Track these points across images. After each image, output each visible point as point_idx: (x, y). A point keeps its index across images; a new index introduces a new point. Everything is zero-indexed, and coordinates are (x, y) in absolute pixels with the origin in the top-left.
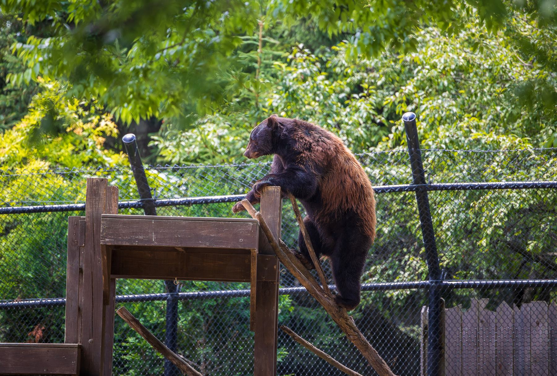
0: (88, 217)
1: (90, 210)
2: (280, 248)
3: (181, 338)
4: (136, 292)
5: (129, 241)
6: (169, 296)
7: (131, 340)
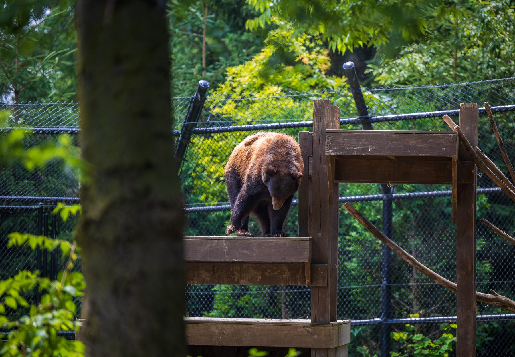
0: (315, 132)
1: (316, 127)
2: (477, 155)
3: (395, 232)
4: (356, 194)
5: (349, 151)
6: (385, 197)
7: (354, 234)
